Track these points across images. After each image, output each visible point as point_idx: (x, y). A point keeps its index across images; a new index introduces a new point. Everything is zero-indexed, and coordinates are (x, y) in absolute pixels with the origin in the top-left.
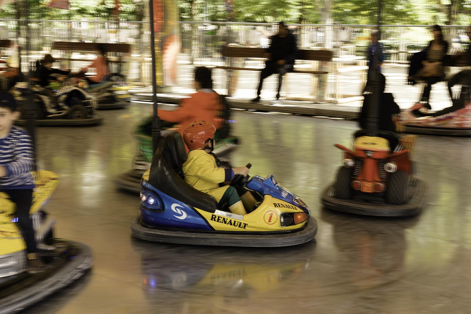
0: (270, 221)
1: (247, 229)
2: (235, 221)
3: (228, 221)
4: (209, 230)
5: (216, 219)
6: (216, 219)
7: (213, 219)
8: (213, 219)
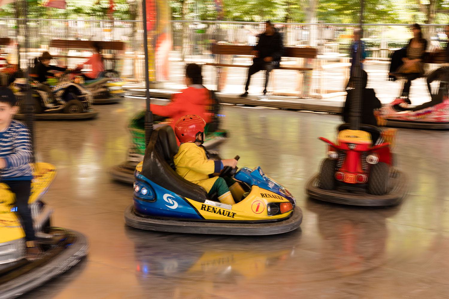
0: (257, 210)
1: (236, 218)
2: (224, 211)
3: (218, 210)
4: (200, 219)
5: (206, 209)
6: (206, 209)
7: (203, 209)
8: (203, 209)
